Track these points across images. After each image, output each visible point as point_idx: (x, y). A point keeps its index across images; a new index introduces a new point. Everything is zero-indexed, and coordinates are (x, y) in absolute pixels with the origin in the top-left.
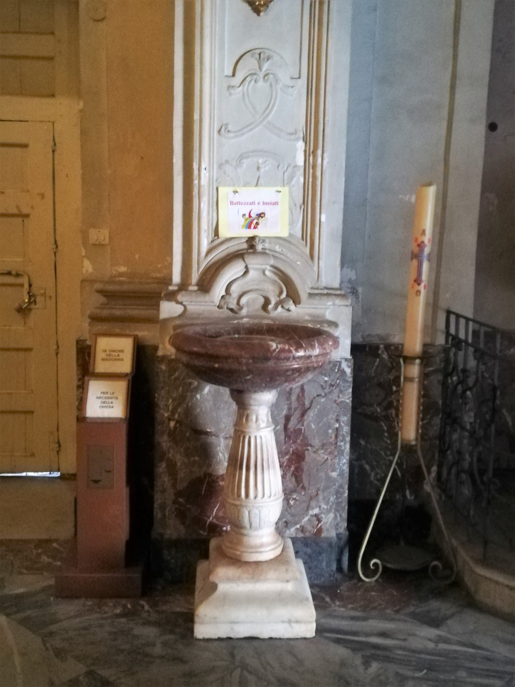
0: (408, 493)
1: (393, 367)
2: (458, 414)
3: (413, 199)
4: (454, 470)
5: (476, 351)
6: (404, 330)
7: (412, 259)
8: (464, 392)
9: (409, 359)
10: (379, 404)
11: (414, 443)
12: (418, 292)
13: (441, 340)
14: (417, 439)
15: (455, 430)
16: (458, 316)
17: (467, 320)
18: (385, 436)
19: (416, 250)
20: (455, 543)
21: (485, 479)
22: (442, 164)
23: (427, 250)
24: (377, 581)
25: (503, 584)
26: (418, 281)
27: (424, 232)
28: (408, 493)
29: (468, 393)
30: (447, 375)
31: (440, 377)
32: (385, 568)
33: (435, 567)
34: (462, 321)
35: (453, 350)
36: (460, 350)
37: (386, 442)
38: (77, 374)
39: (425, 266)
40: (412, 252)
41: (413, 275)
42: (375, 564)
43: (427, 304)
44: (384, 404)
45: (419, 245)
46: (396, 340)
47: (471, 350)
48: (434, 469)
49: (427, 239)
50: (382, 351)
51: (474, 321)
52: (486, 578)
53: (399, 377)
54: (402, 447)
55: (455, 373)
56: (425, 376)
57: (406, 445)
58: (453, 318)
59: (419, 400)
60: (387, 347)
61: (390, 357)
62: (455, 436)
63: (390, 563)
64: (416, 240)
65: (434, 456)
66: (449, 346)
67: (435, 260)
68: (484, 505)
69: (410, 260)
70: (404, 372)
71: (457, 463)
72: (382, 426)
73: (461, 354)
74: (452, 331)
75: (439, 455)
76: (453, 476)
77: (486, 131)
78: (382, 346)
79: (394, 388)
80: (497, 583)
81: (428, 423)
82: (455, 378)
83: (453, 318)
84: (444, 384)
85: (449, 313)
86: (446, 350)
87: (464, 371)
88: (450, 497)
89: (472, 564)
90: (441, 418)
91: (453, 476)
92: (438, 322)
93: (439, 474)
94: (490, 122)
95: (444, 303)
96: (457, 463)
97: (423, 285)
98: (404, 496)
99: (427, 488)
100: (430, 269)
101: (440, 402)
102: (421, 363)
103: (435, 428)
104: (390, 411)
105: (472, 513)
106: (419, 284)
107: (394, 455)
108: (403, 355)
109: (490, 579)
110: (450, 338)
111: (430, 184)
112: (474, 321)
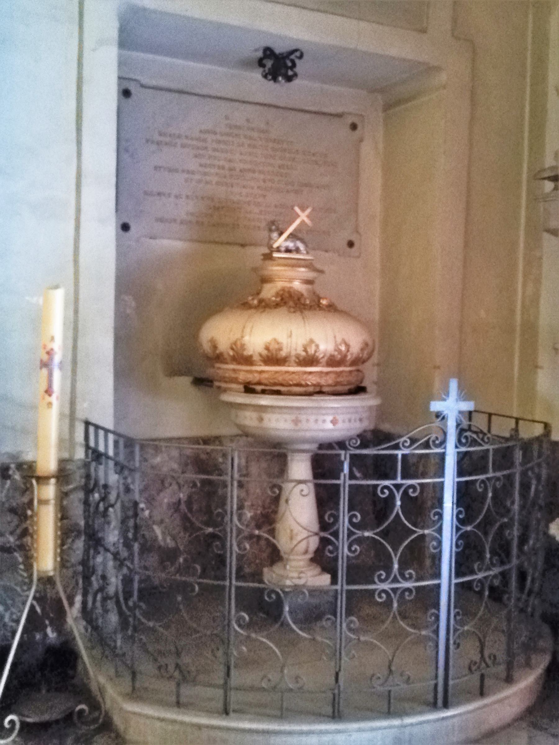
0: (49, 630)
1: (27, 489)
2: (100, 535)
3: (41, 301)
4: (99, 597)
5: (116, 464)
6: (36, 446)
7: (41, 368)
8: (106, 509)
9: (42, 480)
10: (12, 533)
11: (51, 574)
12: (50, 404)
13: (80, 454)
14: (55, 569)
15: (99, 553)
16: (97, 427)
17: (107, 431)
18: (21, 569)
19: (45, 357)
20: (102, 680)
21: (131, 603)
22: (71, 265)
23: (57, 358)
24: (14, 741)
25: (153, 718)
26: (49, 392)
27: (52, 339)
28: (49, 630)
29: (111, 509)
30: (88, 491)
31: (81, 495)
32: (24, 725)
33: (81, 712)
34: (101, 433)
35: (94, 464)
36: (101, 464)
37: (21, 576)
38: (547, 87)
39: (57, 375)
40: (41, 361)
41: (44, 386)
42: (12, 722)
43: (61, 415)
44: (18, 531)
45: (48, 353)
46: (29, 457)
47: (111, 464)
48: (78, 599)
49: (57, 346)
50: (14, 471)
51: (114, 433)
52: (134, 713)
53: (31, 502)
54: (39, 580)
55: (96, 489)
56: (62, 496)
57: (43, 575)
58: (92, 429)
59: (56, 523)
60: (20, 466)
61: (24, 477)
62: (99, 559)
63: (28, 717)
64: (45, 347)
65: (77, 584)
66: (89, 460)
67: (69, 368)
68: (130, 632)
69: (39, 368)
70: (38, 496)
71: (101, 589)
72: (16, 558)
73: (102, 468)
74: (92, 444)
75: (83, 582)
76: (98, 604)
77: (117, 231)
78: (13, 466)
79: (29, 513)
80: (147, 717)
81: (69, 548)
82: (97, 496)
83: (92, 429)
84: (86, 503)
85: (87, 424)
86: (86, 465)
87: (106, 486)
88: (96, 628)
89: (119, 699)
90: (85, 541)
91: (98, 604)
92: (77, 434)
93: (84, 603)
94: (121, 222)
95: (81, 414)
96: (101, 589)
97: (54, 396)
98: (46, 635)
99: (70, 621)
100: (63, 378)
101: (82, 523)
102: (58, 482)
103: (78, 552)
104: (25, 540)
105: (119, 643)
106: (50, 395)
107: (29, 589)
108: (35, 475)
109: (139, 715)
110: (90, 452)
111: (56, 287)
112: (114, 433)
